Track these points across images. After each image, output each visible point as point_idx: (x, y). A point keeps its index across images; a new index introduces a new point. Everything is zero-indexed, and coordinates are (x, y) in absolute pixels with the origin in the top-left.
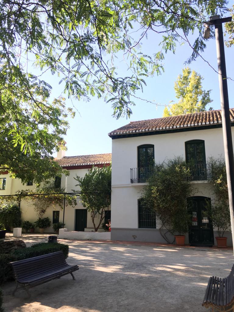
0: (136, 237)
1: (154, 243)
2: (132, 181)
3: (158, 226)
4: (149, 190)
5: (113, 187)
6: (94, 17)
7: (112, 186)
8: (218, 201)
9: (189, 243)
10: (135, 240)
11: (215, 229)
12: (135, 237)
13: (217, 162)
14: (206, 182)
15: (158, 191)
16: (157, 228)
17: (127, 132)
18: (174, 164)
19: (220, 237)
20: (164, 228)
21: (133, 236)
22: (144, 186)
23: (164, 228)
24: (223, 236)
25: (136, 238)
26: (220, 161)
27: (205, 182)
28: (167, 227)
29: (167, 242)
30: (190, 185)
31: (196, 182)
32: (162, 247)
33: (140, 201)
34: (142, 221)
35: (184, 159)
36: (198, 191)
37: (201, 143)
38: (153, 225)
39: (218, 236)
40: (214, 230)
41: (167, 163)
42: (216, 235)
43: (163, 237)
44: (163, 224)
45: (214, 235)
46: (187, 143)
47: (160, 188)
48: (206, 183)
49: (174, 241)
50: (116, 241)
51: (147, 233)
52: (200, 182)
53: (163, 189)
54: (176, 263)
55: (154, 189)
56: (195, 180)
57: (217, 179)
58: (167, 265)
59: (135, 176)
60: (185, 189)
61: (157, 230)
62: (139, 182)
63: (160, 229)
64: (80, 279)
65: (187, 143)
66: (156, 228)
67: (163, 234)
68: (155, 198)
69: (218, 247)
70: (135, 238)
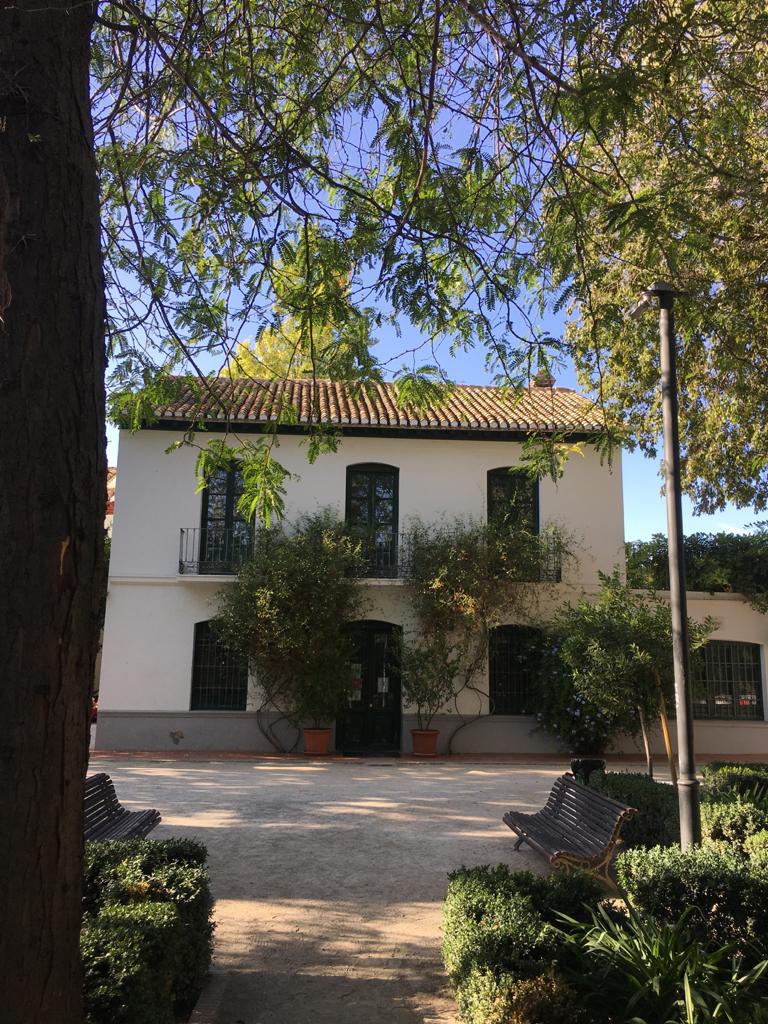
0: (182, 737)
1: (222, 752)
2: (182, 569)
3: (253, 703)
4: (242, 602)
5: (113, 583)
6: (314, 168)
7: (110, 580)
8: (424, 634)
9: (336, 748)
10: (179, 747)
11: (409, 709)
12: (176, 737)
13: (430, 532)
14: (399, 582)
15: (273, 601)
16: (249, 708)
17: (177, 414)
18: (316, 528)
19: (422, 730)
20: (273, 709)
21: (172, 735)
22: (226, 584)
23: (273, 709)
24: (430, 727)
25: (181, 740)
26: (438, 528)
27: (397, 584)
28: (280, 706)
29: (277, 748)
30: (356, 591)
31: (373, 582)
32: (271, 760)
33: (201, 629)
34: (229, 691)
35: (341, 516)
36: (372, 606)
37: (388, 475)
38: (238, 701)
39: (417, 727)
40: (405, 711)
41: (294, 523)
42: (407, 727)
43: (267, 736)
44: (269, 698)
45: (404, 723)
46: (353, 471)
47: (283, 594)
48: (400, 586)
49: (296, 746)
50: (118, 751)
51: (219, 724)
52: (384, 582)
53: (289, 599)
54: (362, 796)
55: (263, 597)
56: (371, 575)
57: (432, 578)
58: (350, 800)
59: (193, 553)
60: (345, 597)
61: (251, 715)
62: (201, 572)
63: (259, 711)
64: (183, 840)
65: (353, 471)
66: (245, 709)
67: (266, 728)
68: (267, 621)
69: (414, 756)
70: (176, 742)
